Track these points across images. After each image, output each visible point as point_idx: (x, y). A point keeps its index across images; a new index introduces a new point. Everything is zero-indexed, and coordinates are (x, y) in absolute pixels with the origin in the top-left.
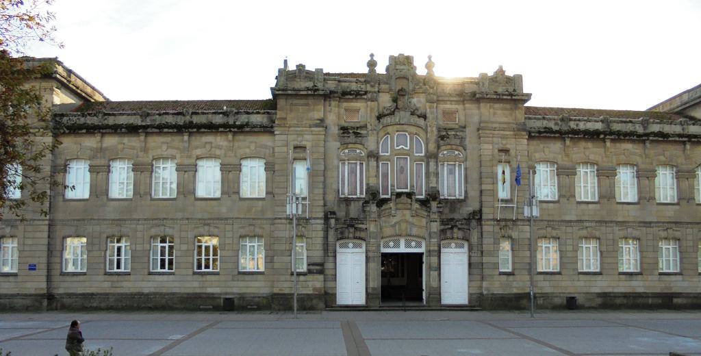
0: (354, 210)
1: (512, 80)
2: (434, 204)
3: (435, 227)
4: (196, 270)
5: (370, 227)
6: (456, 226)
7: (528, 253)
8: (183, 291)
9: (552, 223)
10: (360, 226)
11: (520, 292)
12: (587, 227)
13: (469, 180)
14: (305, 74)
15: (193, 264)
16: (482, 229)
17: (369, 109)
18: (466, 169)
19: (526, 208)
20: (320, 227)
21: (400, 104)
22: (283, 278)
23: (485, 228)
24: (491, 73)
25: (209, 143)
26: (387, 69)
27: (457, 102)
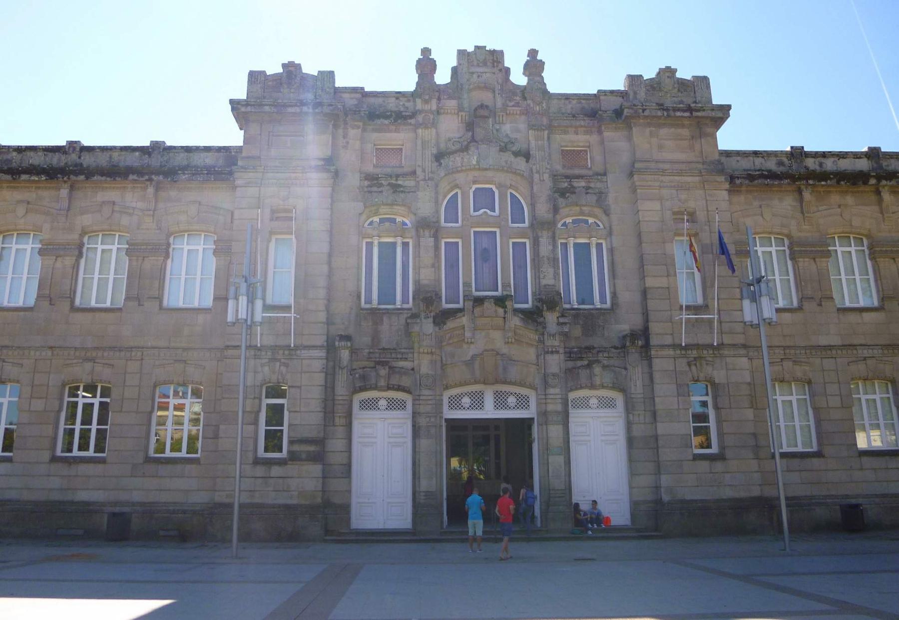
0: (389, 331)
2: (551, 318)
3: (555, 363)
4: (59, 453)
5: (419, 366)
6: (598, 361)
7: (749, 414)
8: (26, 496)
9: (793, 351)
10: (401, 364)
11: (743, 494)
12: (865, 359)
15: (55, 439)
16: (650, 366)
17: (419, 142)
18: (611, 251)
19: (746, 303)
20: (318, 365)
21: (479, 132)
23: (657, 364)
25: (109, 202)
26: (455, 71)
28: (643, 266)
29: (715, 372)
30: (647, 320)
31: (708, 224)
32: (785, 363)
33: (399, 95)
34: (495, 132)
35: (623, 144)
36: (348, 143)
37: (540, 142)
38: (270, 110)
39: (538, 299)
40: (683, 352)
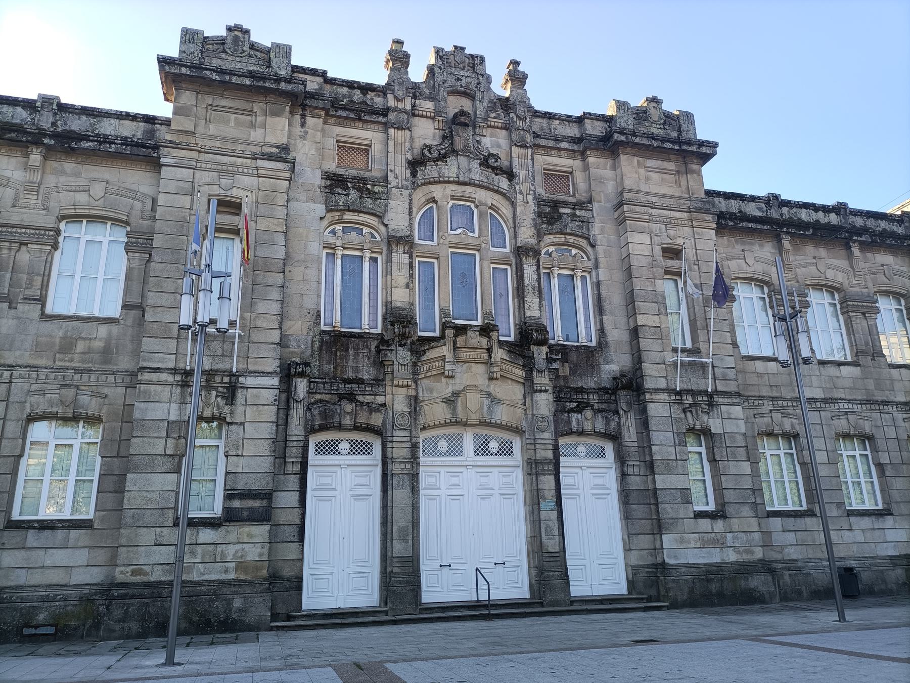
2: (540, 353)
3: (544, 403)
7: (746, 467)
9: (780, 403)
12: (846, 413)
13: (607, 306)
14: (246, 48)
16: (644, 411)
18: (598, 284)
20: (269, 396)
23: (654, 409)
26: (431, 70)
27: (572, 154)
28: (634, 302)
29: (711, 422)
31: (697, 263)
32: (774, 415)
33: (367, 88)
35: (608, 173)
36: (306, 133)
38: (211, 77)
40: (678, 398)
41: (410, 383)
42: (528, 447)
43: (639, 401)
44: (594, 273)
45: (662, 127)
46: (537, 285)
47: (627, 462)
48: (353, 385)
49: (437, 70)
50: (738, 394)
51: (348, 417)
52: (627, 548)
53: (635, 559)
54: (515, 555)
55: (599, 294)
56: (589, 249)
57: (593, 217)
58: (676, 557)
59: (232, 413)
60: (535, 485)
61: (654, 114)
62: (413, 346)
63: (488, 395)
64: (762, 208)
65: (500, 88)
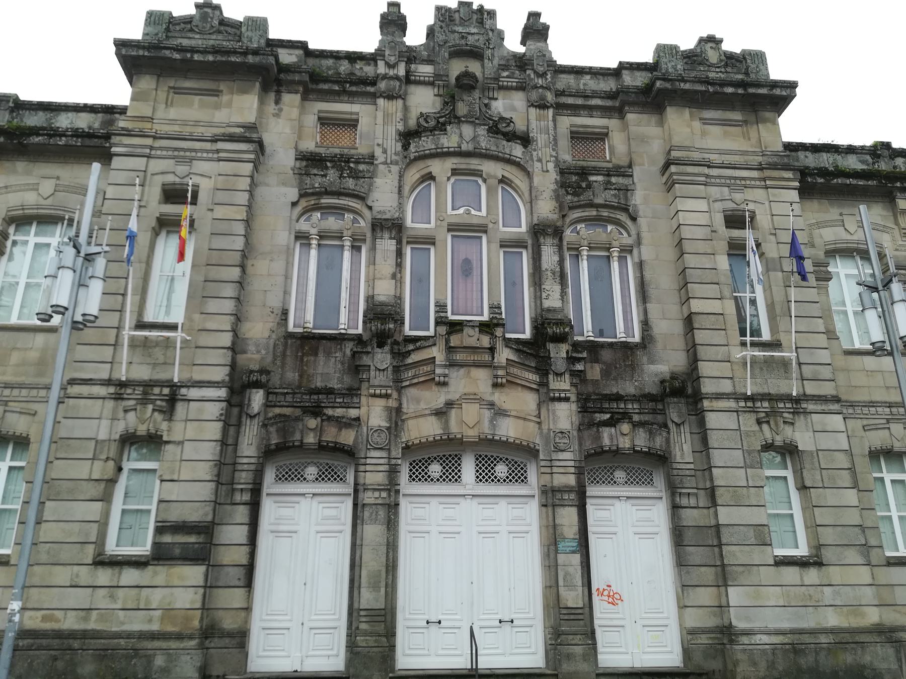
1: (738, 60)
2: (559, 352)
10: (339, 412)
13: (652, 292)
16: (702, 423)
20: (214, 410)
22: (62, 575)
23: (713, 420)
24: (687, 44)
26: (431, 32)
27: (606, 112)
30: (694, 360)
33: (353, 57)
34: (484, 109)
36: (281, 110)
37: (542, 123)
38: (170, 55)
39: (540, 326)
40: (750, 404)
41: (389, 392)
42: (543, 470)
43: (697, 410)
44: (635, 251)
45: (723, 70)
46: (558, 269)
47: (679, 490)
48: (320, 396)
49: (437, 29)
50: (836, 399)
51: (312, 435)
52: (681, 605)
53: (695, 619)
54: (527, 611)
55: (642, 277)
56: (629, 223)
57: (633, 183)
58: (748, 619)
59: (169, 430)
60: (551, 519)
61: (713, 57)
62: (396, 347)
63: (491, 405)
64: (867, 161)
65: (513, 43)
